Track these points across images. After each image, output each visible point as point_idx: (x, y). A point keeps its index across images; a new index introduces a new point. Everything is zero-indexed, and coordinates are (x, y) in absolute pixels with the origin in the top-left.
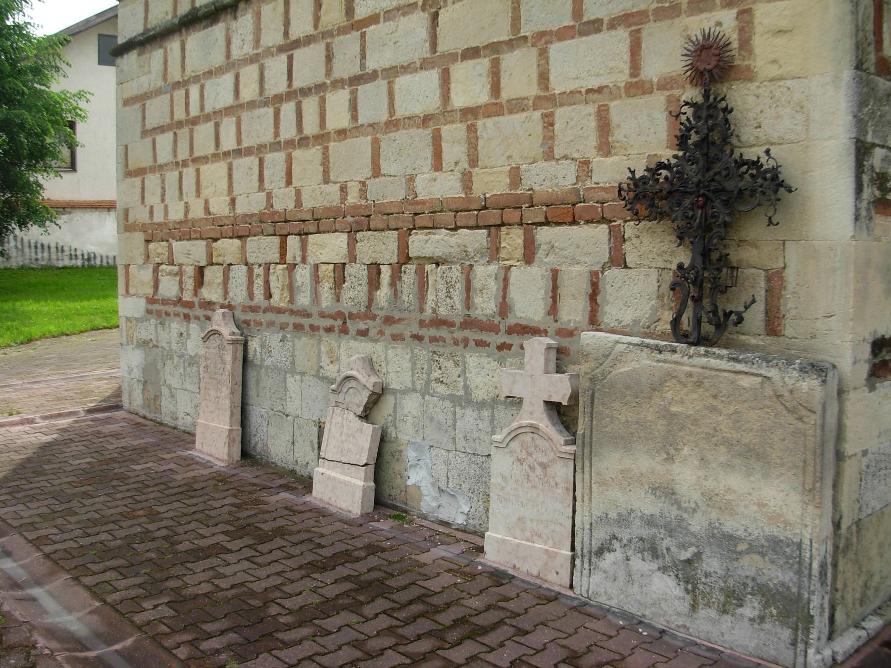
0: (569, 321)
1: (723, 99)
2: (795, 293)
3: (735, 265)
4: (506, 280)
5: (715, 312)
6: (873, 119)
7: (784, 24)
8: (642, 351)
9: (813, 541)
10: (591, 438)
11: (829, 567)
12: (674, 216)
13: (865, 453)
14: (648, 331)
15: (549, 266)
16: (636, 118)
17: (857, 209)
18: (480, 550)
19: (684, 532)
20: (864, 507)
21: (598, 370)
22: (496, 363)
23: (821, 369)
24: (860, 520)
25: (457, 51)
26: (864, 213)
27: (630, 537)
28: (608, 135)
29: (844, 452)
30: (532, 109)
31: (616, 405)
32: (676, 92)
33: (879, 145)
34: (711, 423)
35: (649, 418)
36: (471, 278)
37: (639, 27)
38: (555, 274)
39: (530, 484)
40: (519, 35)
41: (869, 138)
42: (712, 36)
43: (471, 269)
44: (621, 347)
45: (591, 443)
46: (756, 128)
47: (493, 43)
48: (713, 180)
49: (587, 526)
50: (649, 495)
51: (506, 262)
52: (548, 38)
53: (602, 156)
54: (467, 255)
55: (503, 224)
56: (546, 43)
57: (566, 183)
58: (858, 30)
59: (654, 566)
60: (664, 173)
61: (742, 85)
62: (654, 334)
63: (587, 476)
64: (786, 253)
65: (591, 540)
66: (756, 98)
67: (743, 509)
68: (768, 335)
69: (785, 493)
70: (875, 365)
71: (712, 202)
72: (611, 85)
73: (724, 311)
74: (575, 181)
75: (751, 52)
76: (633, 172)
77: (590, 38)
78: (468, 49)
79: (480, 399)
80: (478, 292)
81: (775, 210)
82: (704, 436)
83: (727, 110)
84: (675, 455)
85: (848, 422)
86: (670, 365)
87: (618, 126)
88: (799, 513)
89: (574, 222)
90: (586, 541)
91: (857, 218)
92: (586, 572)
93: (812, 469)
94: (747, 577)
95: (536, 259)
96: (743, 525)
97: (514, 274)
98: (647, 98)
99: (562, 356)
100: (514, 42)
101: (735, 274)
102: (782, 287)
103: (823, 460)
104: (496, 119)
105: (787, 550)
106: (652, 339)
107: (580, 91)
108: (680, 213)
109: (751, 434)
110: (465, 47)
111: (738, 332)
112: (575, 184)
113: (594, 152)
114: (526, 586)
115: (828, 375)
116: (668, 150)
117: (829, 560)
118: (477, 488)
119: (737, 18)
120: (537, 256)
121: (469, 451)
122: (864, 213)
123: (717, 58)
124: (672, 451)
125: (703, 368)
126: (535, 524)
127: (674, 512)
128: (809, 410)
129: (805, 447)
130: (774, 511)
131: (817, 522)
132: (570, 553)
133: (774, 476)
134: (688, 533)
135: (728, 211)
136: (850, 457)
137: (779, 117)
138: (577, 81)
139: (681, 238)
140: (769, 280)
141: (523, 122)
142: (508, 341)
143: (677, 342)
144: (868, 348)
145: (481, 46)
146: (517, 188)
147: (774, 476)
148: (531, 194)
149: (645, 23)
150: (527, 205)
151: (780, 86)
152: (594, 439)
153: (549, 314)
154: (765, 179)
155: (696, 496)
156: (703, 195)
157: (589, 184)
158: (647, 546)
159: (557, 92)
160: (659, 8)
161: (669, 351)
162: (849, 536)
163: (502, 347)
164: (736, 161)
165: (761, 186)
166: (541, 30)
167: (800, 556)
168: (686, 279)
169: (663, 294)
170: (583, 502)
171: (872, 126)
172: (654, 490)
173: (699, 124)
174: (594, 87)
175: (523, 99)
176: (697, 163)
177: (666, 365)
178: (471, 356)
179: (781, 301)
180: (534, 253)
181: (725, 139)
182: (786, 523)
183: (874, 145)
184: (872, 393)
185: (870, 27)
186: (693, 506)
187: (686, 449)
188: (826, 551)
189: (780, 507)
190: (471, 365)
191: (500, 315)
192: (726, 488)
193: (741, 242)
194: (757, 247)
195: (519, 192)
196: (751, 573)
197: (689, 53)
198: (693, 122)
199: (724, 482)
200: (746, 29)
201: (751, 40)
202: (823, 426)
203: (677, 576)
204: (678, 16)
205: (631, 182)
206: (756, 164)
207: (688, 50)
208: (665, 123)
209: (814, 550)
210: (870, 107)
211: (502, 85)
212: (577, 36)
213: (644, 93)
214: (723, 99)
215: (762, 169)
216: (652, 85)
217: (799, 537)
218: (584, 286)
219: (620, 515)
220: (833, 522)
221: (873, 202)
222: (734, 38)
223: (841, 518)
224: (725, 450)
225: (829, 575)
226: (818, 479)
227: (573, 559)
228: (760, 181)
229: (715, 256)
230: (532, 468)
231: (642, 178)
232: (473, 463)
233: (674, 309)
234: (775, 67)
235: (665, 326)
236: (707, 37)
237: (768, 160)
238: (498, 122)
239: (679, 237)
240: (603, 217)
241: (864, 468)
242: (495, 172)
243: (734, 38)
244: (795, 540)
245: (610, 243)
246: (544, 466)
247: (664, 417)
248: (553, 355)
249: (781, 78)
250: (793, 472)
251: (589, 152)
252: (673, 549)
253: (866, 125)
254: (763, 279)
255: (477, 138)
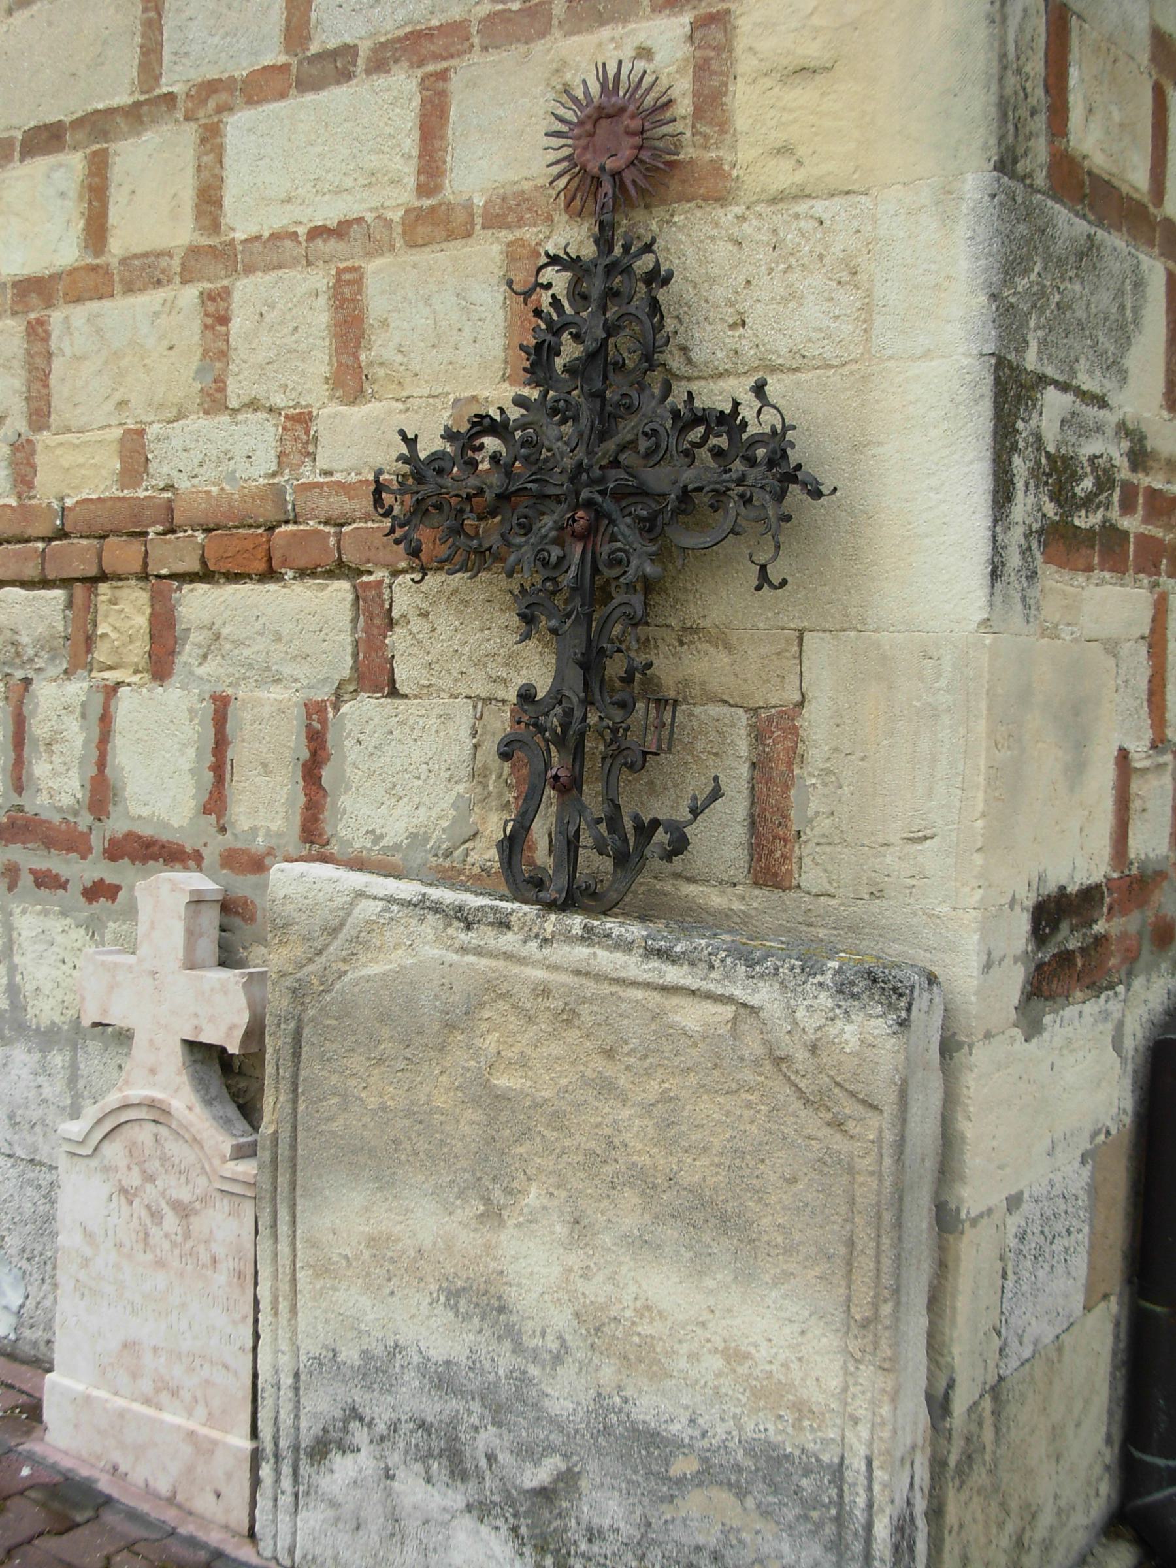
0: (254, 830)
1: (648, 248)
2: (829, 772)
3: (672, 694)
4: (106, 719)
5: (613, 820)
6: (1042, 311)
7: (812, 51)
8: (422, 920)
9: (876, 1464)
10: (293, 1147)
11: (921, 1523)
12: (512, 558)
13: (1014, 1202)
14: (447, 864)
15: (207, 687)
16: (427, 301)
17: (997, 548)
18: (34, 1411)
19: (531, 1415)
20: (1014, 1343)
21: (311, 968)
22: (82, 931)
23: (894, 989)
24: (1001, 1379)
25: (14, 133)
26: (1014, 560)
27: (394, 1416)
28: (358, 346)
29: (958, 1210)
30: (177, 279)
31: (356, 1062)
32: (529, 234)
33: (1056, 383)
34: (598, 1125)
35: (440, 1102)
36: (26, 712)
37: (445, 64)
38: (221, 707)
39: (149, 1257)
40: (158, 92)
41: (1031, 360)
42: (624, 85)
43: (26, 689)
44: (368, 909)
45: (293, 1160)
46: (733, 326)
47: (97, 112)
48: (615, 463)
49: (287, 1381)
50: (439, 1309)
51: (107, 674)
52: (223, 97)
53: (342, 403)
54: (18, 654)
55: (103, 577)
56: (220, 110)
57: (255, 472)
58: (1005, 68)
59: (456, 1499)
60: (491, 443)
61: (699, 214)
62: (461, 872)
63: (284, 1247)
64: (806, 664)
65: (297, 1417)
66: (735, 249)
67: (683, 1363)
68: (756, 884)
69: (796, 1328)
70: (1040, 967)
71: (612, 522)
72: (369, 217)
73: (636, 818)
74: (274, 468)
75: (723, 125)
76: (411, 442)
77: (324, 95)
78: (37, 128)
79: (45, 1022)
80: (42, 749)
81: (778, 547)
82: (581, 1158)
83: (658, 278)
84: (505, 1207)
85: (968, 1128)
86: (493, 963)
87: (384, 323)
88: (834, 1383)
89: (270, 575)
90: (286, 1418)
91: (996, 573)
92: (286, 1500)
93: (872, 1265)
94: (698, 1549)
95: (177, 668)
96: (687, 1407)
97: (126, 704)
98: (457, 249)
99: (237, 921)
100: (145, 109)
101: (667, 717)
102: (795, 756)
103: (900, 1239)
104: (93, 306)
105: (804, 1482)
106: (453, 887)
107: (295, 233)
108: (527, 553)
109: (704, 1161)
110: (32, 124)
111: (677, 876)
112: (274, 475)
113: (323, 390)
114: (135, 1531)
115: (914, 1009)
116: (506, 384)
117: (920, 1505)
118: (39, 1248)
119: (691, 38)
120: (180, 659)
121: (20, 1153)
122: (1014, 560)
123: (637, 140)
124: (497, 1195)
125: (577, 973)
126: (163, 1360)
127: (506, 1360)
128: (864, 1102)
129: (852, 1202)
130: (769, 1375)
131: (885, 1410)
132: (247, 1445)
133: (767, 1278)
134: (542, 1418)
135: (654, 549)
136: (974, 1222)
137: (792, 296)
138: (289, 207)
139: (528, 619)
140: (759, 735)
141: (156, 314)
142: (110, 879)
143: (515, 899)
144: (1022, 923)
145: (67, 120)
146: (136, 484)
147: (767, 1278)
148: (170, 501)
149: (460, 54)
150: (160, 528)
151: (797, 216)
152: (300, 1152)
153: (206, 810)
154: (752, 462)
155: (561, 1319)
156: (589, 504)
157: (309, 475)
158: (437, 1444)
159: (240, 236)
160: (496, 14)
161: (492, 924)
162: (974, 1427)
163: (98, 891)
164: (676, 414)
165: (740, 481)
166: (209, 77)
167: (840, 1503)
168: (541, 729)
169: (485, 767)
170: (276, 1314)
171: (1038, 327)
172: (453, 1296)
173: (584, 314)
174: (328, 223)
175: (159, 255)
176: (576, 419)
177: (484, 963)
178: (24, 912)
179: (792, 792)
180: (173, 653)
181: (650, 358)
182: (801, 1409)
183: (1042, 380)
184: (1035, 1041)
185: (1036, 66)
186: (554, 1346)
187: (534, 1190)
188: (912, 1484)
189: (785, 1365)
190: (24, 933)
191: (91, 809)
192: (639, 1304)
193: (688, 633)
194: (729, 647)
195: (142, 494)
196: (710, 1538)
197: (564, 128)
198: (569, 310)
199: (633, 1288)
200: (715, 65)
201: (725, 94)
202: (900, 1144)
203: (514, 1530)
204: (543, 34)
205: (406, 468)
206: (729, 421)
207: (562, 120)
208: (501, 314)
209: (877, 1488)
210: (1033, 277)
211: (113, 219)
212: (293, 91)
213: (450, 236)
214: (648, 248)
215: (745, 436)
216: (472, 215)
217: (839, 1450)
218: (294, 744)
219: (366, 1355)
220: (929, 1398)
221: (1040, 532)
222: (682, 89)
223: (951, 1385)
224: (636, 1200)
225: (921, 1547)
226: (886, 1293)
227: (256, 1458)
228: (738, 466)
229: (615, 668)
230: (155, 1215)
231: (436, 457)
232: (30, 1182)
233: (513, 806)
234: (787, 164)
235: (486, 854)
236: (610, 86)
237: (759, 412)
238: (98, 315)
239: (522, 616)
240: (340, 563)
241: (1013, 1242)
242: (87, 443)
243: (682, 89)
244: (826, 1458)
245: (355, 628)
246: (184, 1211)
247: (476, 1101)
248: (210, 918)
249: (801, 194)
250: (817, 1271)
251: (309, 391)
252: (504, 1457)
253: (1024, 324)
254: (743, 732)
255: (49, 356)
